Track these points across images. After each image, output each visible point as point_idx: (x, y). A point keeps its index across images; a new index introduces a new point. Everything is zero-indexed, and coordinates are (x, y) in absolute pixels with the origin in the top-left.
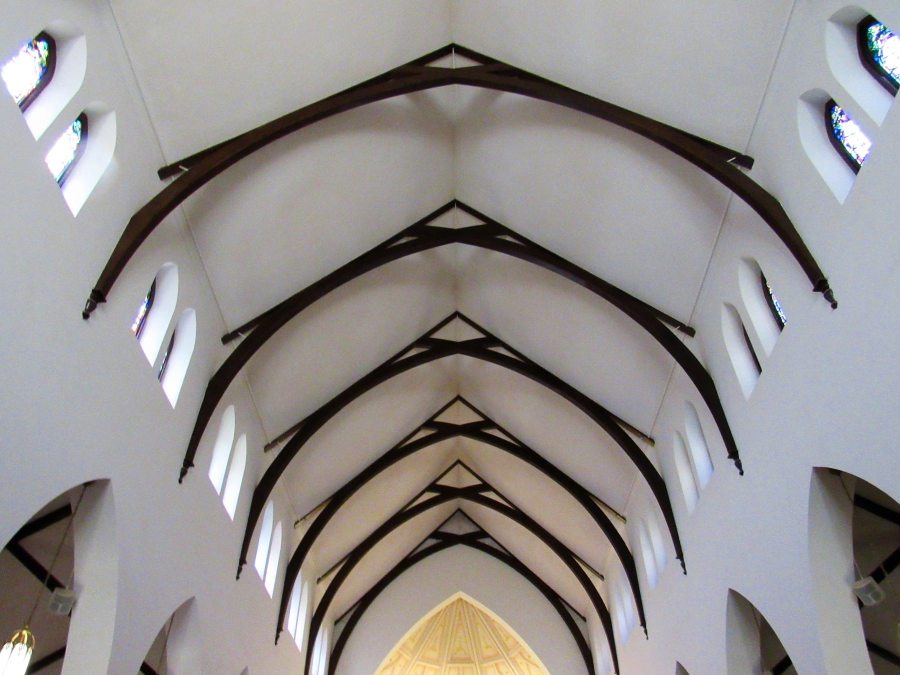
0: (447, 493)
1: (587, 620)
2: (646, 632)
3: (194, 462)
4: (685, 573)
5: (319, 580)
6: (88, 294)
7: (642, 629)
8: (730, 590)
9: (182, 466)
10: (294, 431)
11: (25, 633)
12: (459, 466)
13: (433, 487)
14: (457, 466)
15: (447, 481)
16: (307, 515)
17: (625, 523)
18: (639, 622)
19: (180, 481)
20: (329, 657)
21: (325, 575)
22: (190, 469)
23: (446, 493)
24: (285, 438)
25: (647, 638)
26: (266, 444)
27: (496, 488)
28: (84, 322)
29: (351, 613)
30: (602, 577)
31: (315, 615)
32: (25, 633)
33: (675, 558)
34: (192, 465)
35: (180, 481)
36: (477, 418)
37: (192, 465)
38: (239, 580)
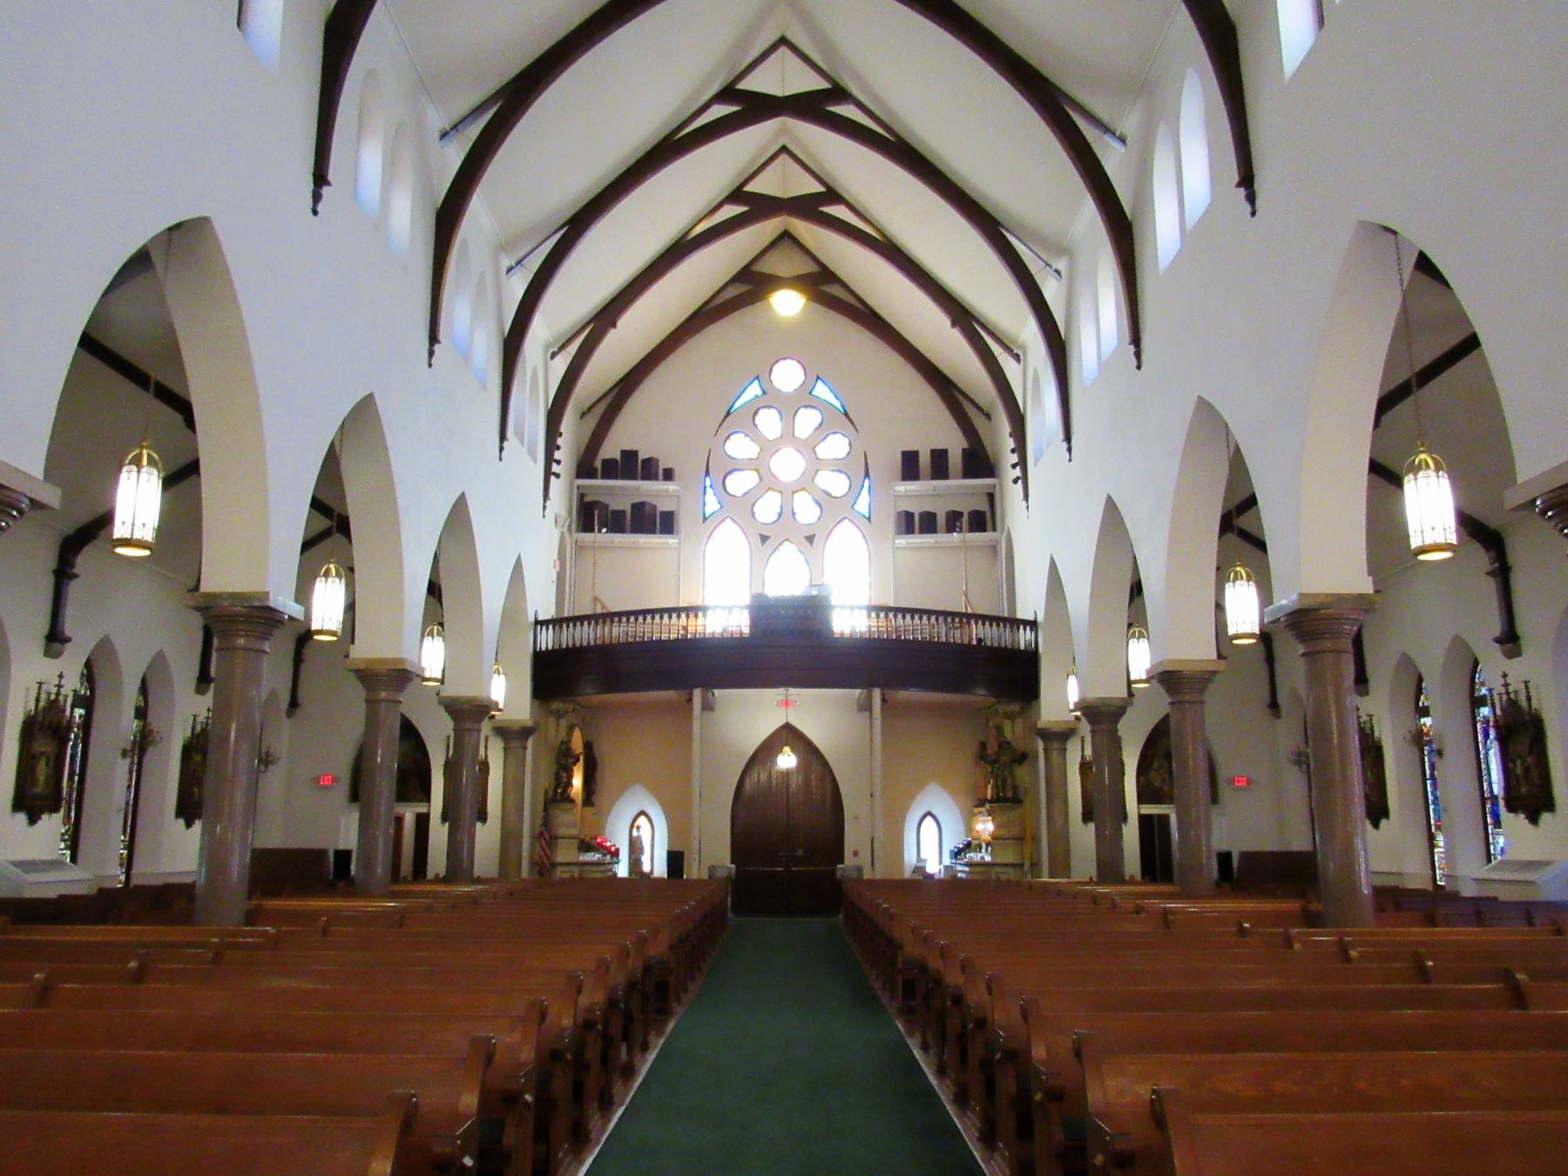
0: (757, 108)
1: (992, 417)
2: (1069, 450)
3: (331, 177)
4: (1070, 460)
5: (553, 355)
6: (310, 179)
7: (1065, 445)
8: (1200, 399)
9: (311, 186)
10: (488, 109)
11: (332, 566)
12: (784, 158)
13: (737, 196)
14: (782, 156)
15: (760, 82)
16: (460, 122)
17: (1059, 281)
18: (1061, 435)
19: (315, 212)
20: (575, 465)
21: (562, 348)
22: (325, 191)
23: (760, 207)
24: (475, 119)
25: (1070, 460)
26: (581, 412)
27: (851, 200)
28: (430, 369)
29: (609, 400)
30: (1017, 358)
31: (509, 334)
32: (332, 566)
33: (1126, 344)
34: (438, 342)
35: (315, 212)
36: (819, 84)
37: (438, 342)
38: (433, 367)
